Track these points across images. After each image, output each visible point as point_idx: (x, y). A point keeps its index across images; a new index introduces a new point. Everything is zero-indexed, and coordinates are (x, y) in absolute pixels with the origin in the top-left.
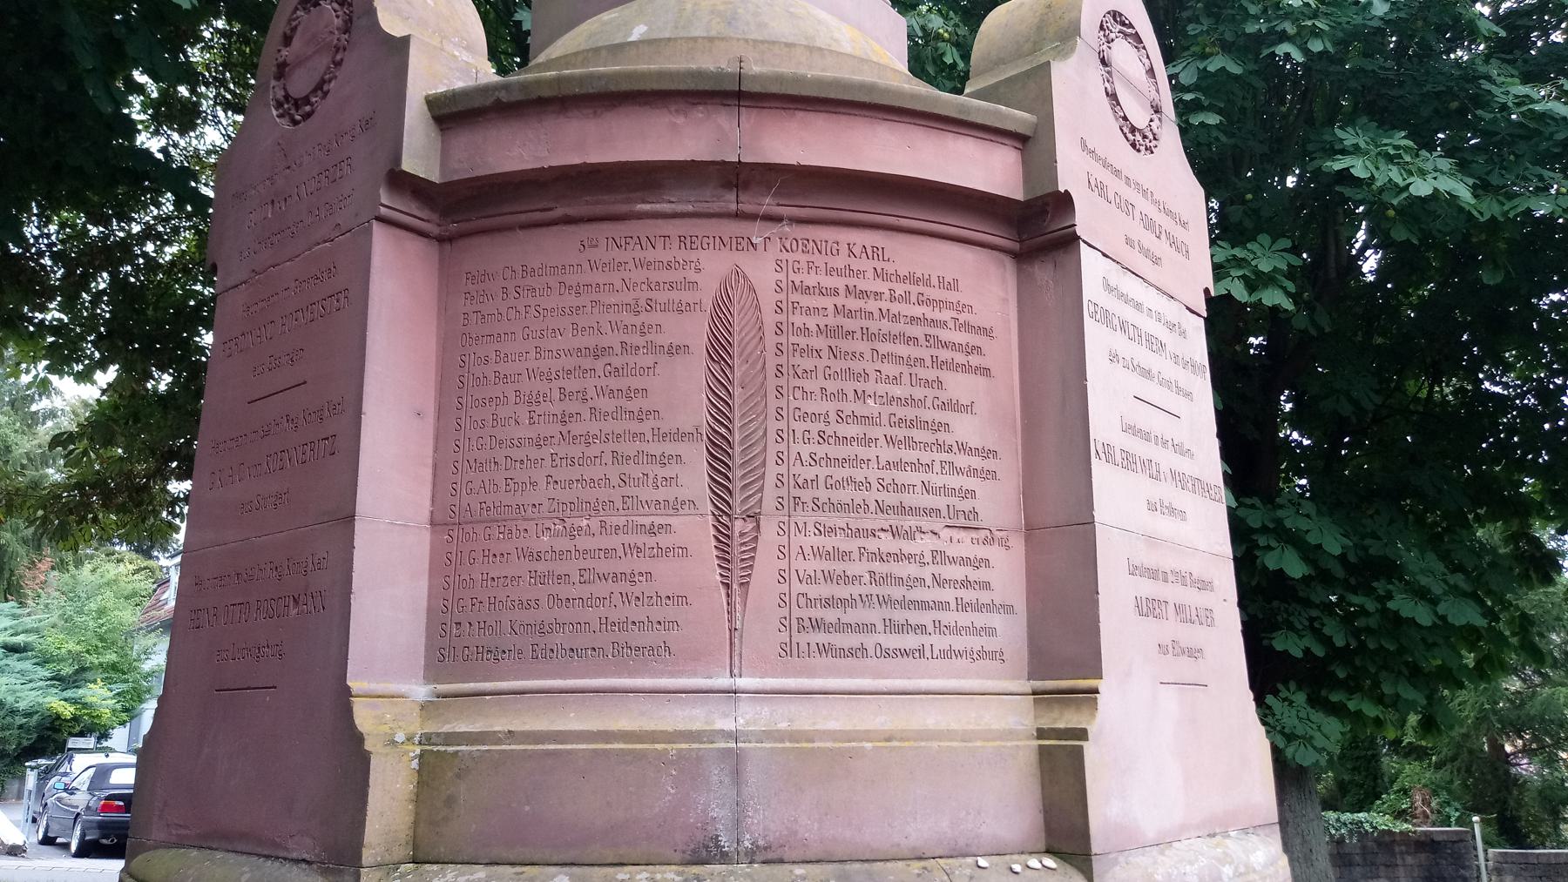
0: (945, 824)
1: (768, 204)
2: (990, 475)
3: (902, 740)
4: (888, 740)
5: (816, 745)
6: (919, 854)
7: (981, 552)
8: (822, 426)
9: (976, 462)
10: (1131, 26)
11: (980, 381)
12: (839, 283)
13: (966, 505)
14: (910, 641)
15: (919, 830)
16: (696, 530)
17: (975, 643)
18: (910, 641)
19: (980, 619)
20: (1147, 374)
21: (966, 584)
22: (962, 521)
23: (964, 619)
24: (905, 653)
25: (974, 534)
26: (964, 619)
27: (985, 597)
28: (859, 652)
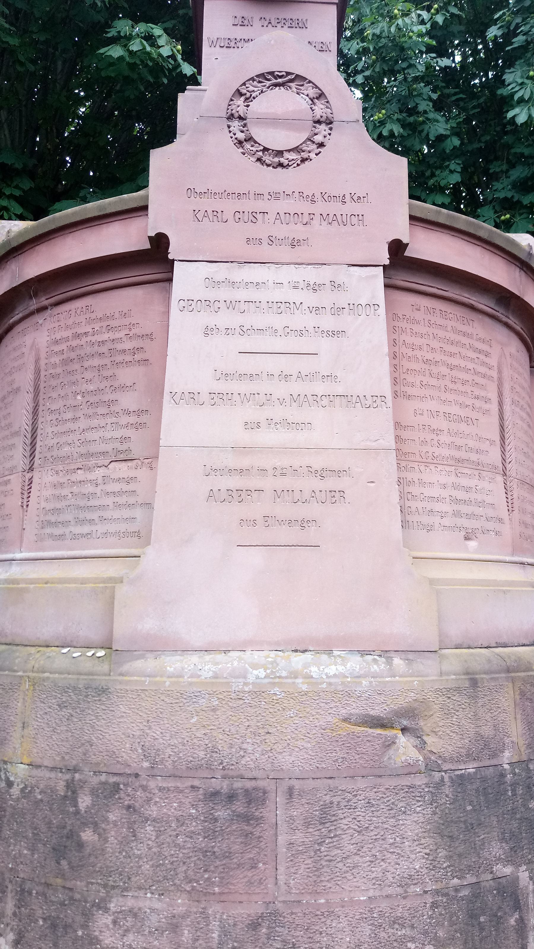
0: (61, 629)
1: (34, 304)
2: (486, 412)
3: (52, 583)
4: (46, 583)
5: (20, 586)
6: (48, 644)
7: (132, 473)
8: (57, 416)
9: (133, 419)
10: (288, 74)
11: (140, 370)
12: (68, 333)
13: (124, 447)
14: (86, 529)
15: (47, 631)
16: (16, 482)
17: (123, 527)
18: (86, 529)
19: (126, 513)
20: (243, 331)
21: (121, 493)
22: (122, 457)
23: (117, 514)
24: (83, 536)
25: (130, 464)
26: (117, 514)
27: (132, 500)
28: (61, 537)
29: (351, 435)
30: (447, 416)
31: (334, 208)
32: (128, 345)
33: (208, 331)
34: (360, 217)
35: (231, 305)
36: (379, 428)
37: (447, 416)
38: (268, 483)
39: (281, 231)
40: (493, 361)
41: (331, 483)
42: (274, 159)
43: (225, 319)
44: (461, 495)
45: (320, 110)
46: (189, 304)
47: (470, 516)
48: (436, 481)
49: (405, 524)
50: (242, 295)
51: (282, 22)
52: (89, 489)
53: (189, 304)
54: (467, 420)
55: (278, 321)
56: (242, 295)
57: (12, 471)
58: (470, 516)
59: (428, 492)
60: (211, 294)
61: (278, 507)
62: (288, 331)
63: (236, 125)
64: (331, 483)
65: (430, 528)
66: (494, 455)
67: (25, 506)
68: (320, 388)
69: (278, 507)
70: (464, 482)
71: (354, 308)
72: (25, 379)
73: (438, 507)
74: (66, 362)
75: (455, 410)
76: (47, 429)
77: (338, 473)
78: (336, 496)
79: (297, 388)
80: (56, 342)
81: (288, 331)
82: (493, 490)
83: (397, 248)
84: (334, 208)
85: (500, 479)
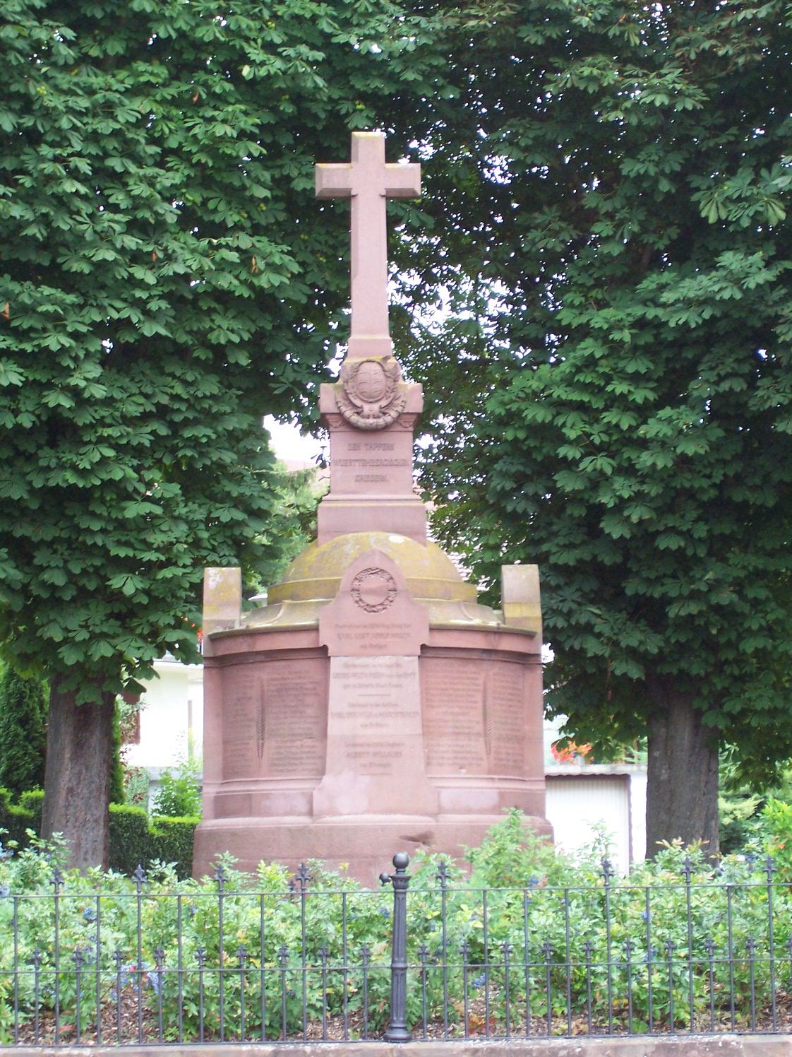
29: (405, 729)
30: (452, 713)
31: (397, 631)
32: (310, 686)
33: (346, 687)
34: (408, 635)
35: (355, 675)
36: (414, 726)
37: (452, 713)
38: (371, 750)
39: (375, 642)
40: (481, 681)
41: (396, 749)
42: (371, 609)
43: (352, 681)
44: (457, 749)
45: (391, 585)
46: (337, 676)
47: (464, 758)
48: (445, 745)
49: (428, 764)
50: (359, 670)
51: (378, 446)
52: (294, 750)
53: (337, 676)
54: (464, 714)
55: (374, 681)
56: (359, 670)
57: (250, 738)
58: (464, 758)
59: (442, 749)
60: (346, 671)
61: (376, 759)
62: (378, 686)
63: (355, 594)
64: (396, 749)
65: (441, 765)
66: (479, 728)
67: (260, 756)
68: (391, 710)
69: (376, 759)
70: (461, 743)
71: (406, 675)
72: (254, 693)
73: (446, 755)
74: (278, 690)
75: (456, 710)
76: (270, 722)
77: (398, 745)
78: (398, 754)
79: (381, 710)
80: (273, 680)
81: (378, 686)
82: (478, 746)
83: (423, 647)
84: (397, 631)
85: (482, 740)
